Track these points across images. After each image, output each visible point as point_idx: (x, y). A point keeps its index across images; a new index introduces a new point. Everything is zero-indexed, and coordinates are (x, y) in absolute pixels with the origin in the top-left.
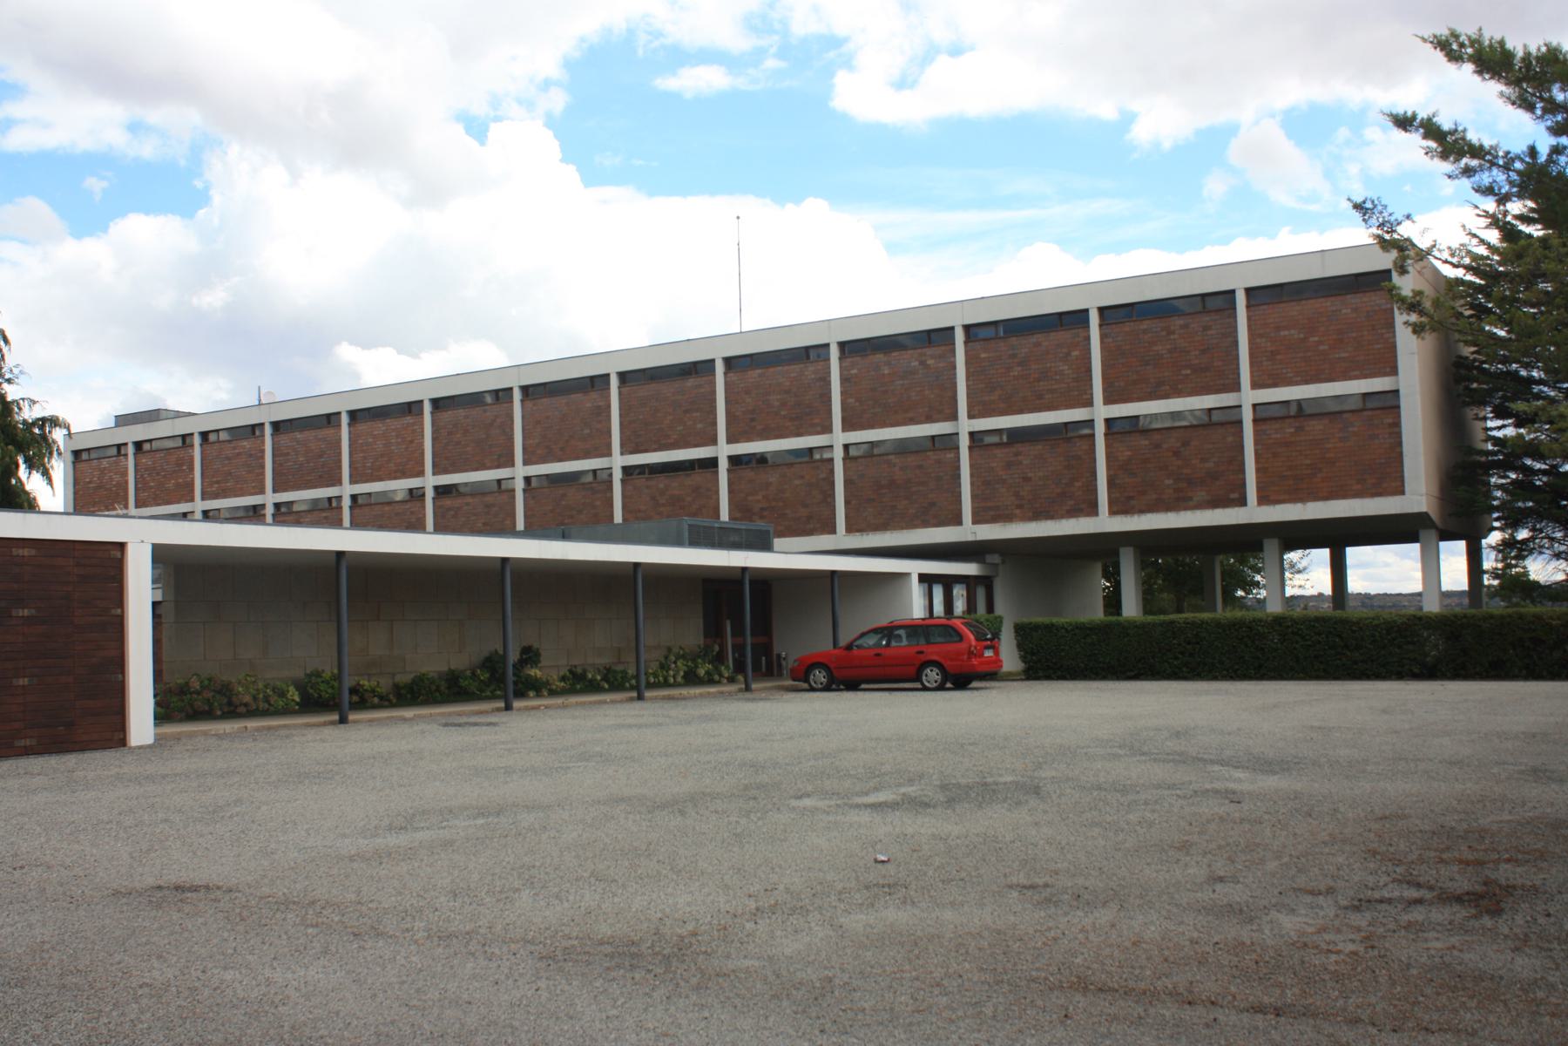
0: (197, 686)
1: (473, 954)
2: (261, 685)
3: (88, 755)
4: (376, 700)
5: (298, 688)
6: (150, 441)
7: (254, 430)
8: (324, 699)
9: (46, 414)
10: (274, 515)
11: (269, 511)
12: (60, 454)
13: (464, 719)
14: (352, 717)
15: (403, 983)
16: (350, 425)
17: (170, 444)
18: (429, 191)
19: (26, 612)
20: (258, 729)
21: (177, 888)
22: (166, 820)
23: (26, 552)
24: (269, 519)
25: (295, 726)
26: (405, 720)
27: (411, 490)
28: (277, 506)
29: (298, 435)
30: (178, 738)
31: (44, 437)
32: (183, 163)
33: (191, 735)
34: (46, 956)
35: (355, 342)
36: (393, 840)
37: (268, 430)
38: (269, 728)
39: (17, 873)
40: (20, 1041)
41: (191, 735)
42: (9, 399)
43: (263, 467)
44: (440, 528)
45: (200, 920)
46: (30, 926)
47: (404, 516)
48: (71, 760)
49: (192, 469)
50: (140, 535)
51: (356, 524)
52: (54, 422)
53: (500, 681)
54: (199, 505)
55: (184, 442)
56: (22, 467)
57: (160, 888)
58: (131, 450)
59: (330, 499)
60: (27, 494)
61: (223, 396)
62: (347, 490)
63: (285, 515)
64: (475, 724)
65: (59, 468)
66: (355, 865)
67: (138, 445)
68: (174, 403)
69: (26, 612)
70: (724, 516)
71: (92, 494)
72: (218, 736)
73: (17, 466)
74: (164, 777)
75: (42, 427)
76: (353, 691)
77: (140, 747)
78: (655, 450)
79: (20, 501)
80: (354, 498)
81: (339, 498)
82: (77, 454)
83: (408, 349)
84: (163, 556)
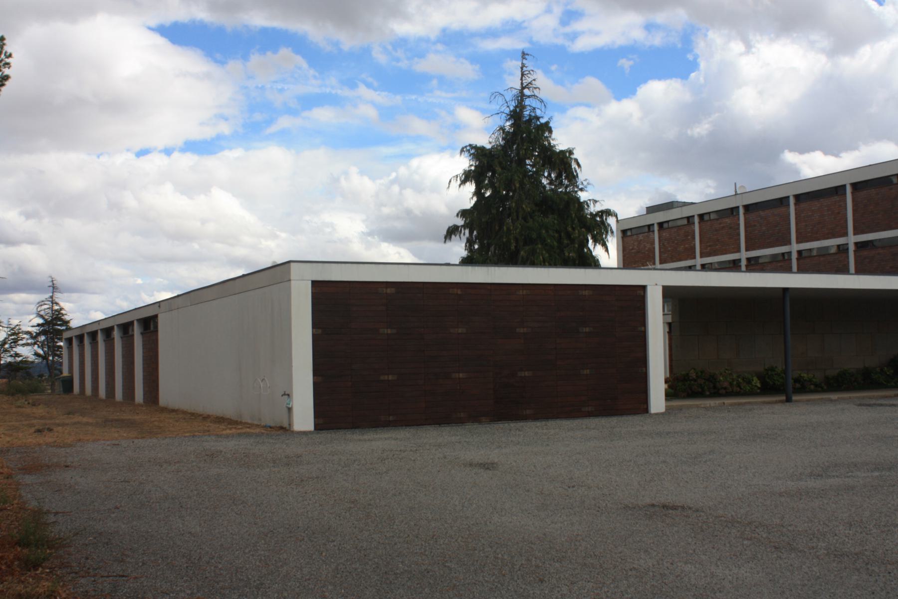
0: (694, 375)
1: (858, 570)
2: (735, 376)
3: (625, 418)
4: (812, 387)
5: (759, 378)
6: (668, 222)
7: (733, 211)
8: (774, 386)
9: (604, 208)
10: (747, 266)
11: (744, 263)
12: (612, 232)
13: (873, 402)
14: (794, 398)
15: (804, 585)
16: (795, 204)
17: (680, 223)
18: (845, 41)
19: (587, 330)
20: (731, 405)
21: (665, 507)
22: (664, 462)
23: (586, 293)
24: (743, 268)
25: (756, 403)
26: (831, 400)
27: (839, 246)
28: (749, 260)
29: (762, 213)
30: (680, 409)
31: (603, 222)
32: (679, 46)
33: (689, 407)
34: (578, 544)
35: (791, 150)
36: (812, 483)
37: (741, 211)
38: (739, 404)
39: (570, 490)
40: (554, 597)
41: (689, 407)
42: (582, 200)
43: (739, 234)
44: (860, 271)
45: (676, 529)
46: (572, 524)
47: (834, 263)
48: (614, 420)
49: (694, 238)
50: (655, 281)
51: (802, 270)
52: (608, 213)
54: (699, 261)
55: (688, 221)
56: (591, 241)
57: (653, 505)
58: (656, 228)
59: (783, 254)
60: (593, 257)
61: (712, 191)
62: (795, 247)
63: (754, 265)
64: (881, 405)
65: (613, 243)
66: (783, 499)
67: (661, 225)
68: (681, 198)
69: (587, 330)
71: (632, 258)
72: (706, 408)
73: (588, 241)
74: (668, 433)
75: (601, 217)
76: (796, 380)
77: (657, 414)
79: (590, 262)
80: (800, 252)
81: (790, 253)
82: (624, 232)
83: (832, 150)
84: (669, 293)
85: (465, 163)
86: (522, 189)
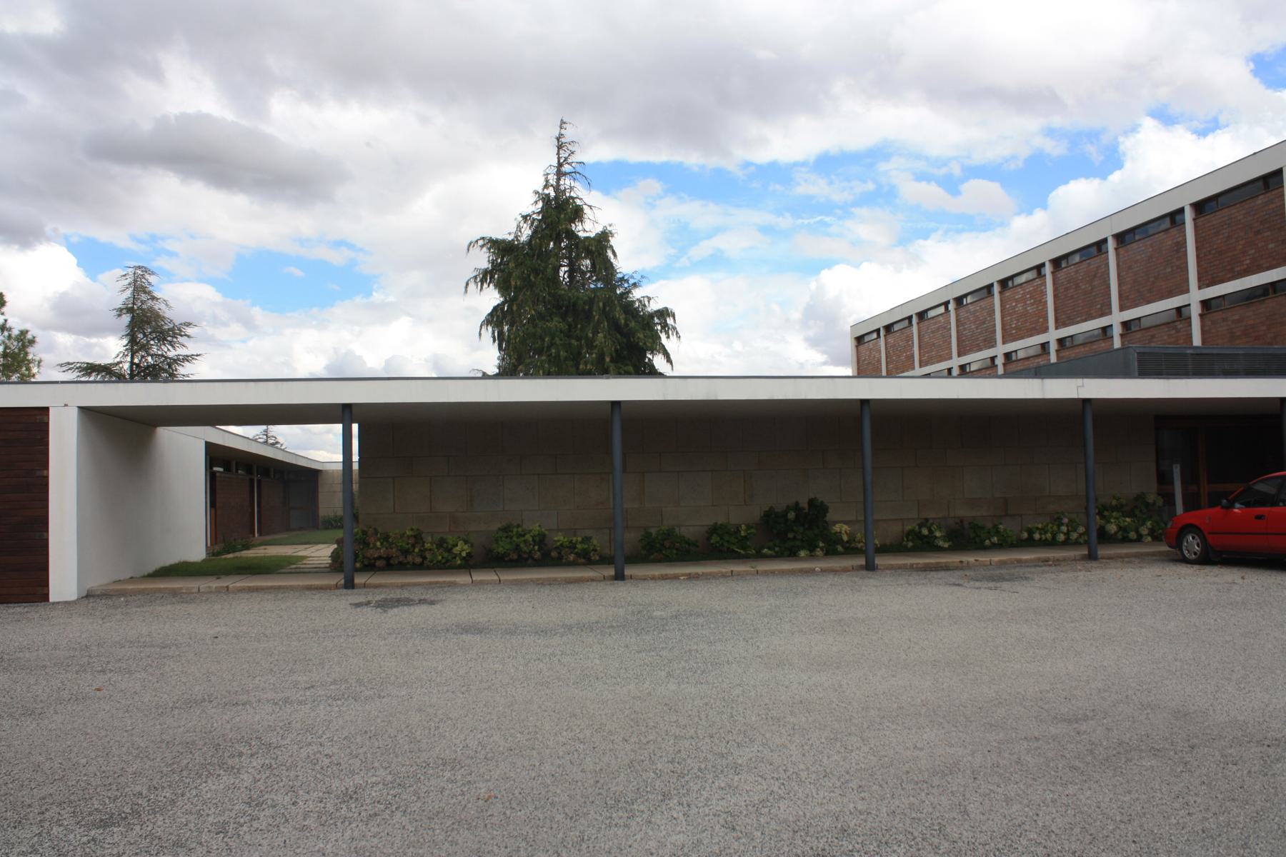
4: (572, 557)
14: (628, 572)
16: (1000, 293)
51: (1008, 375)
53: (793, 535)
62: (1000, 349)
70: (1197, 340)
77: (58, 603)
78: (1229, 280)
85: (483, 260)
86: (557, 289)
